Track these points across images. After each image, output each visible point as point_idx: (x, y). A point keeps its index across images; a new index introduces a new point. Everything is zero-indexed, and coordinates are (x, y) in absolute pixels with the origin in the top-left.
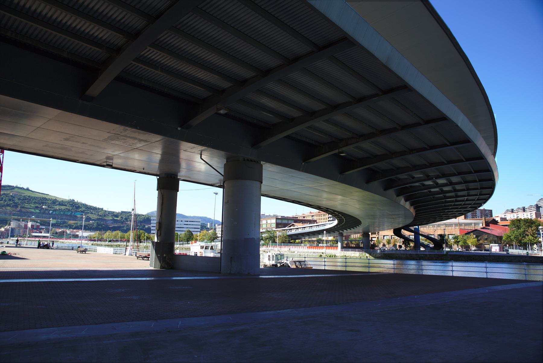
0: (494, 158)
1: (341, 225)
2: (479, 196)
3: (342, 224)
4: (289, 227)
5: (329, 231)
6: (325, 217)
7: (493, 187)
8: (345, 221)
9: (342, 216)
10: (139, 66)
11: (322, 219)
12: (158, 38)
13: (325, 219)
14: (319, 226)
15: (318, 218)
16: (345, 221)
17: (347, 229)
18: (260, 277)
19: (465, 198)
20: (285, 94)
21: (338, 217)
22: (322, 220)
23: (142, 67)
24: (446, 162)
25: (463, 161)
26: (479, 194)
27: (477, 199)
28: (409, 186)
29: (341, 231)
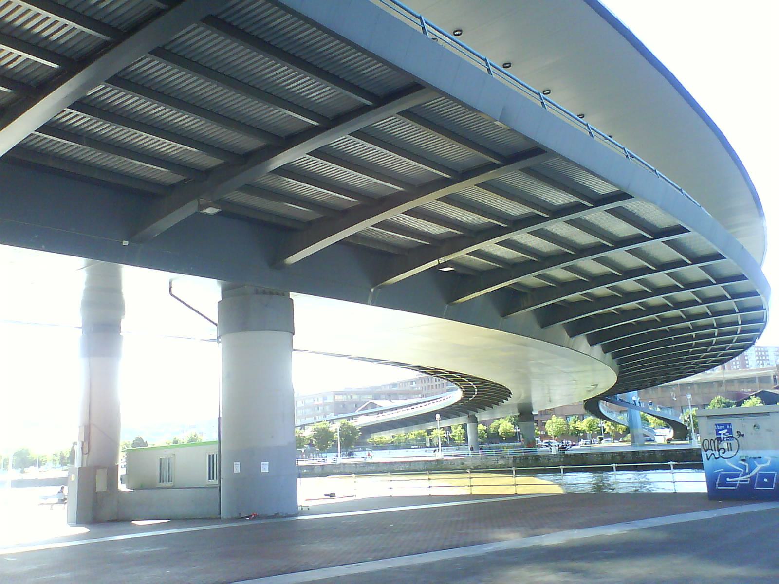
0: (67, 106)
1: (471, 399)
2: (739, 334)
3: (472, 397)
4: (363, 410)
5: (448, 413)
6: (425, 385)
7: (764, 320)
8: (476, 390)
9: (470, 380)
10: (20, 56)
11: (433, 388)
12: (173, 39)
13: (436, 385)
14: (437, 400)
15: (425, 385)
16: (476, 390)
17: (485, 407)
18: (299, 518)
19: (712, 341)
20: (202, 92)
21: (461, 384)
22: (434, 390)
23: (11, 53)
24: (682, 287)
25: (711, 284)
26: (741, 331)
27: (737, 340)
28: (634, 321)
29: (472, 413)
